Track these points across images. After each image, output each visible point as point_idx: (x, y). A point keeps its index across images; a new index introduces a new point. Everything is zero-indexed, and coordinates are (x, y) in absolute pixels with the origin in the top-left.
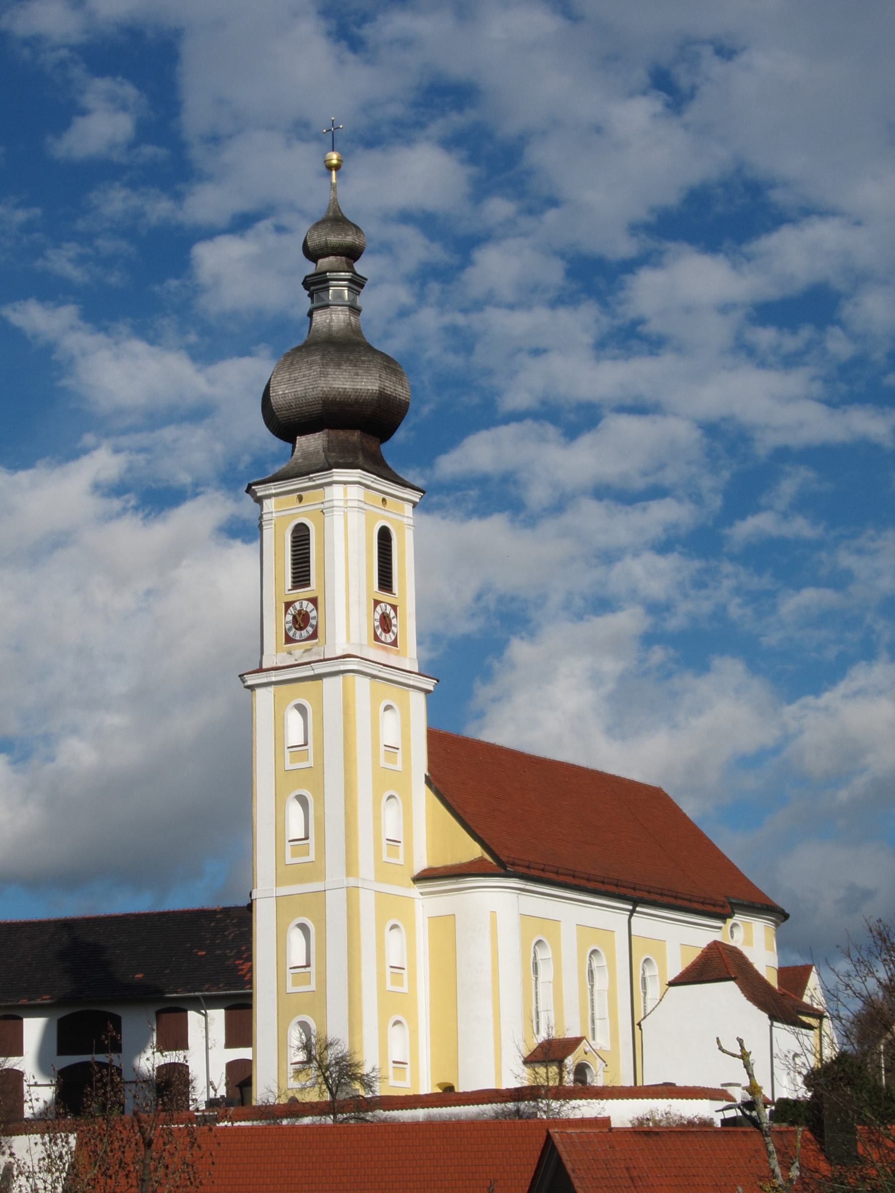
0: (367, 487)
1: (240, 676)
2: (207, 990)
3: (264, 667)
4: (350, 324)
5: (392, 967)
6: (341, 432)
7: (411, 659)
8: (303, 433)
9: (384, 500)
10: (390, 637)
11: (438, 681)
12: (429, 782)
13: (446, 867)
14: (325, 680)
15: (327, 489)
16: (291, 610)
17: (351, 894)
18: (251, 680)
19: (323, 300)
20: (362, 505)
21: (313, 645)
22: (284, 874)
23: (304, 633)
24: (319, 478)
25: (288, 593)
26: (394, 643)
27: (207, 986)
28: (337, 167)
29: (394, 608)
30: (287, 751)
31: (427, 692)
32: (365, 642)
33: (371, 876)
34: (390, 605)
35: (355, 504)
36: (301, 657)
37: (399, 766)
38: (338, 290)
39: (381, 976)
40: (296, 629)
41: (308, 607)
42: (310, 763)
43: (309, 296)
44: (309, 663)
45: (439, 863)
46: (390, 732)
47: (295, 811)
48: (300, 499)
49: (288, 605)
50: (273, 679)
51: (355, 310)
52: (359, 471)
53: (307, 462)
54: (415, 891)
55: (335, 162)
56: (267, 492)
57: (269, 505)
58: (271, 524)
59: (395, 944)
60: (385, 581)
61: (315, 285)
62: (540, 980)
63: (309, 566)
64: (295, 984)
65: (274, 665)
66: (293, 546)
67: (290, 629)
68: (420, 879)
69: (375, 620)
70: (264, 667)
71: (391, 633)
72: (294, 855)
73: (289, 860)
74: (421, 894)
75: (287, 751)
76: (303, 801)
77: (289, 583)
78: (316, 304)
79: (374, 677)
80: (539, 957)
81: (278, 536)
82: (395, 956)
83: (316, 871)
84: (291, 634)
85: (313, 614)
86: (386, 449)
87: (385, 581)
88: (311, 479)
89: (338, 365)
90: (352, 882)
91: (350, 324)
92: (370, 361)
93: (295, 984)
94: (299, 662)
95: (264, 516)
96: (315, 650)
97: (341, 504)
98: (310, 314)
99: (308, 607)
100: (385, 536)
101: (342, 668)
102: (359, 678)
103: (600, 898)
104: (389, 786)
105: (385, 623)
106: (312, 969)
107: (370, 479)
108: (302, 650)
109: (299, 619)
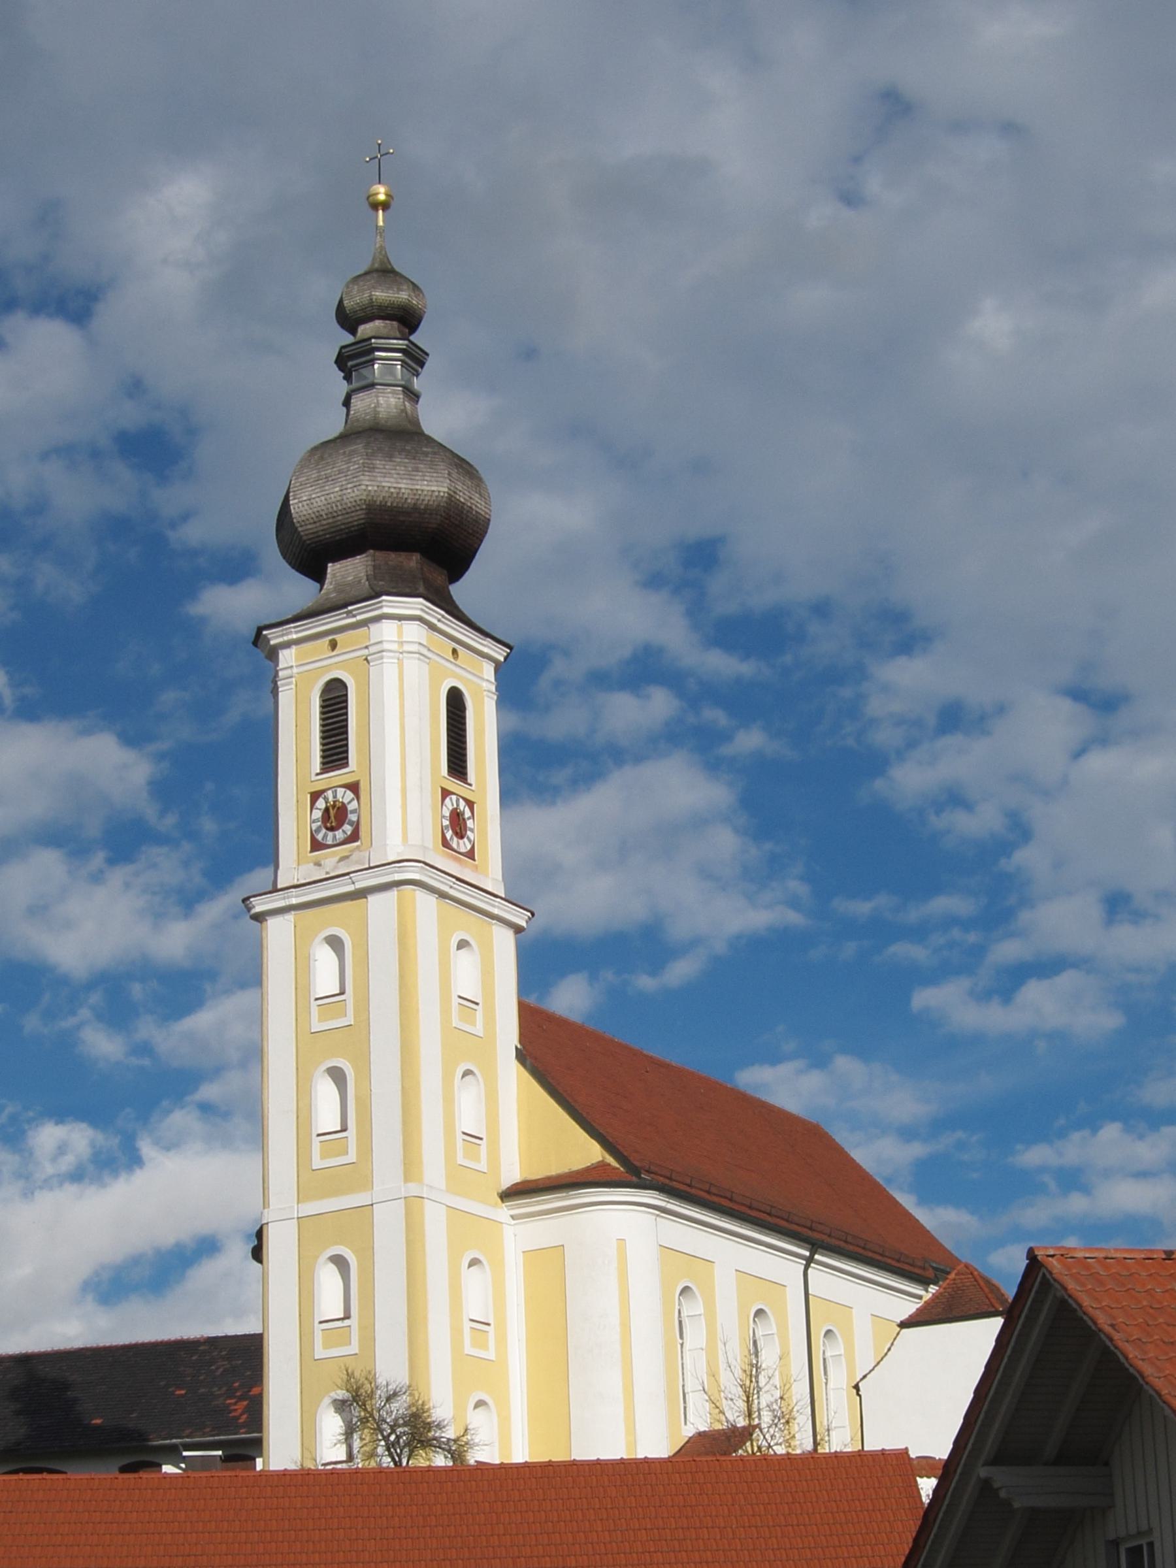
0: (432, 627)
1: (244, 900)
2: (188, 1437)
3: (279, 886)
4: (404, 411)
5: (464, 1133)
6: (393, 555)
7: (494, 879)
8: (335, 559)
9: (454, 651)
10: (464, 846)
11: (533, 914)
12: (521, 1056)
13: (549, 1178)
14: (372, 898)
15: (374, 627)
16: (321, 804)
17: (412, 1208)
18: (260, 905)
19: (366, 378)
20: (425, 652)
21: (352, 851)
22: (310, 1184)
23: (339, 835)
24: (362, 612)
25: (314, 778)
26: (471, 854)
27: (187, 1432)
28: (385, 206)
29: (470, 804)
30: (314, 1004)
31: (518, 930)
32: (430, 845)
33: (442, 1184)
34: (465, 799)
35: (415, 648)
36: (335, 868)
37: (478, 1029)
38: (387, 364)
39: (456, 1331)
40: (327, 829)
41: (345, 796)
42: (349, 1019)
43: (345, 378)
44: (348, 874)
45: (537, 1173)
46: (466, 975)
47: (326, 1093)
48: (333, 645)
49: (315, 796)
50: (294, 901)
51: (412, 395)
52: (421, 600)
53: (342, 596)
54: (504, 1212)
55: (382, 197)
56: (286, 638)
57: (286, 658)
58: (290, 683)
59: (475, 1284)
60: (457, 764)
61: (352, 361)
62: (687, 1346)
63: (347, 739)
64: (326, 1346)
65: (296, 882)
66: (322, 713)
67: (318, 830)
68: (511, 1194)
69: (443, 817)
70: (279, 886)
71: (465, 840)
72: (323, 1156)
73: (317, 1163)
74: (513, 1217)
75: (314, 1004)
76: (337, 1076)
77: (317, 765)
78: (355, 385)
79: (443, 895)
80: (684, 1314)
81: (300, 702)
82: (476, 1304)
83: (359, 1175)
84: (319, 837)
85: (353, 806)
86: (456, 590)
87: (457, 764)
88: (350, 614)
89: (390, 457)
90: (413, 1189)
91: (404, 411)
92: (435, 453)
93: (326, 1346)
94: (332, 874)
95: (281, 674)
96: (354, 857)
97: (395, 647)
98: (347, 403)
99: (345, 796)
100: (456, 703)
101: (398, 877)
102: (420, 895)
103: (767, 1235)
104: (466, 1062)
105: (458, 823)
106: (354, 1322)
107: (436, 615)
108: (337, 858)
109: (332, 813)
